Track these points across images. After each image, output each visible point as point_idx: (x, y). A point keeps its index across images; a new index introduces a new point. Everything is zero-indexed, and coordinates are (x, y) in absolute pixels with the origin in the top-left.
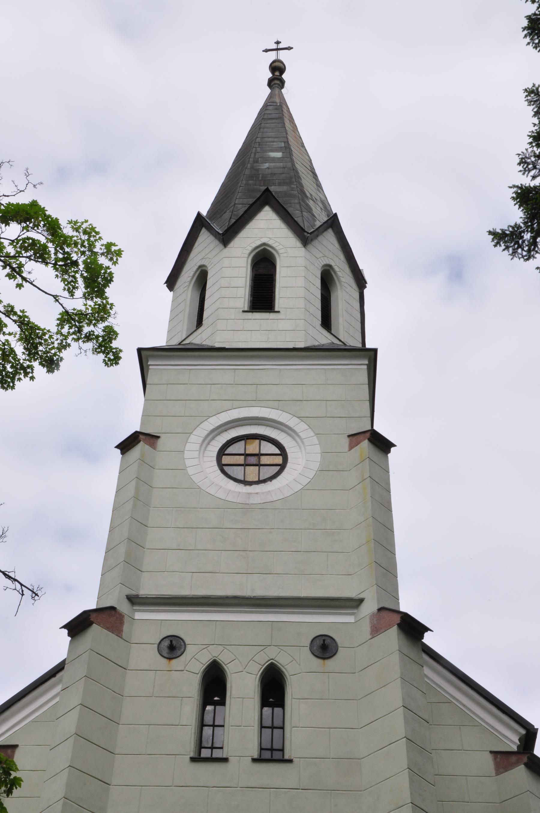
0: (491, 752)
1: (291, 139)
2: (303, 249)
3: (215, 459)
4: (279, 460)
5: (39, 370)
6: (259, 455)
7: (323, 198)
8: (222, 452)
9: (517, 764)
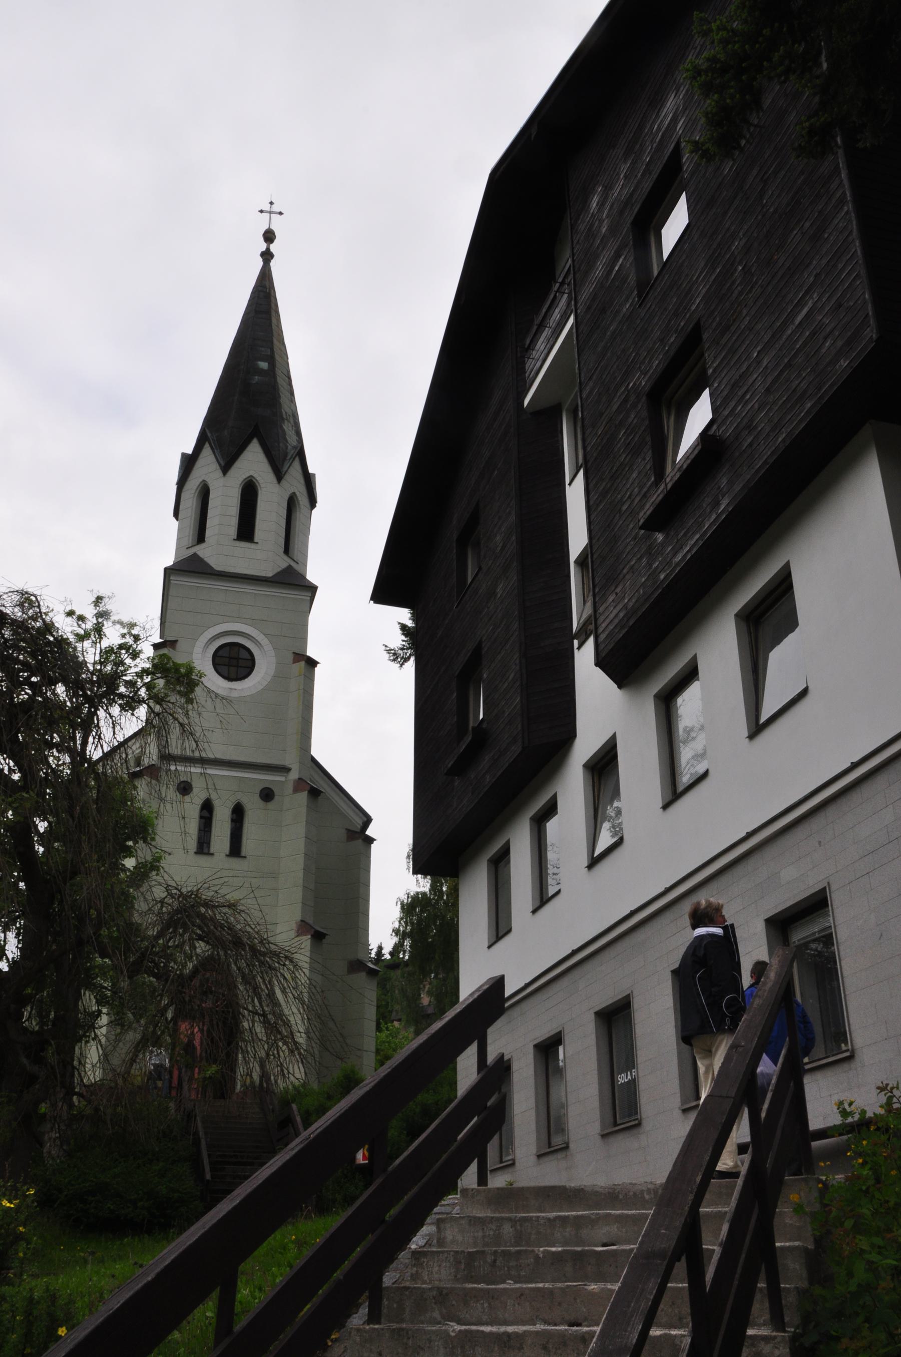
0: (346, 829)
2: (277, 485)
3: (211, 659)
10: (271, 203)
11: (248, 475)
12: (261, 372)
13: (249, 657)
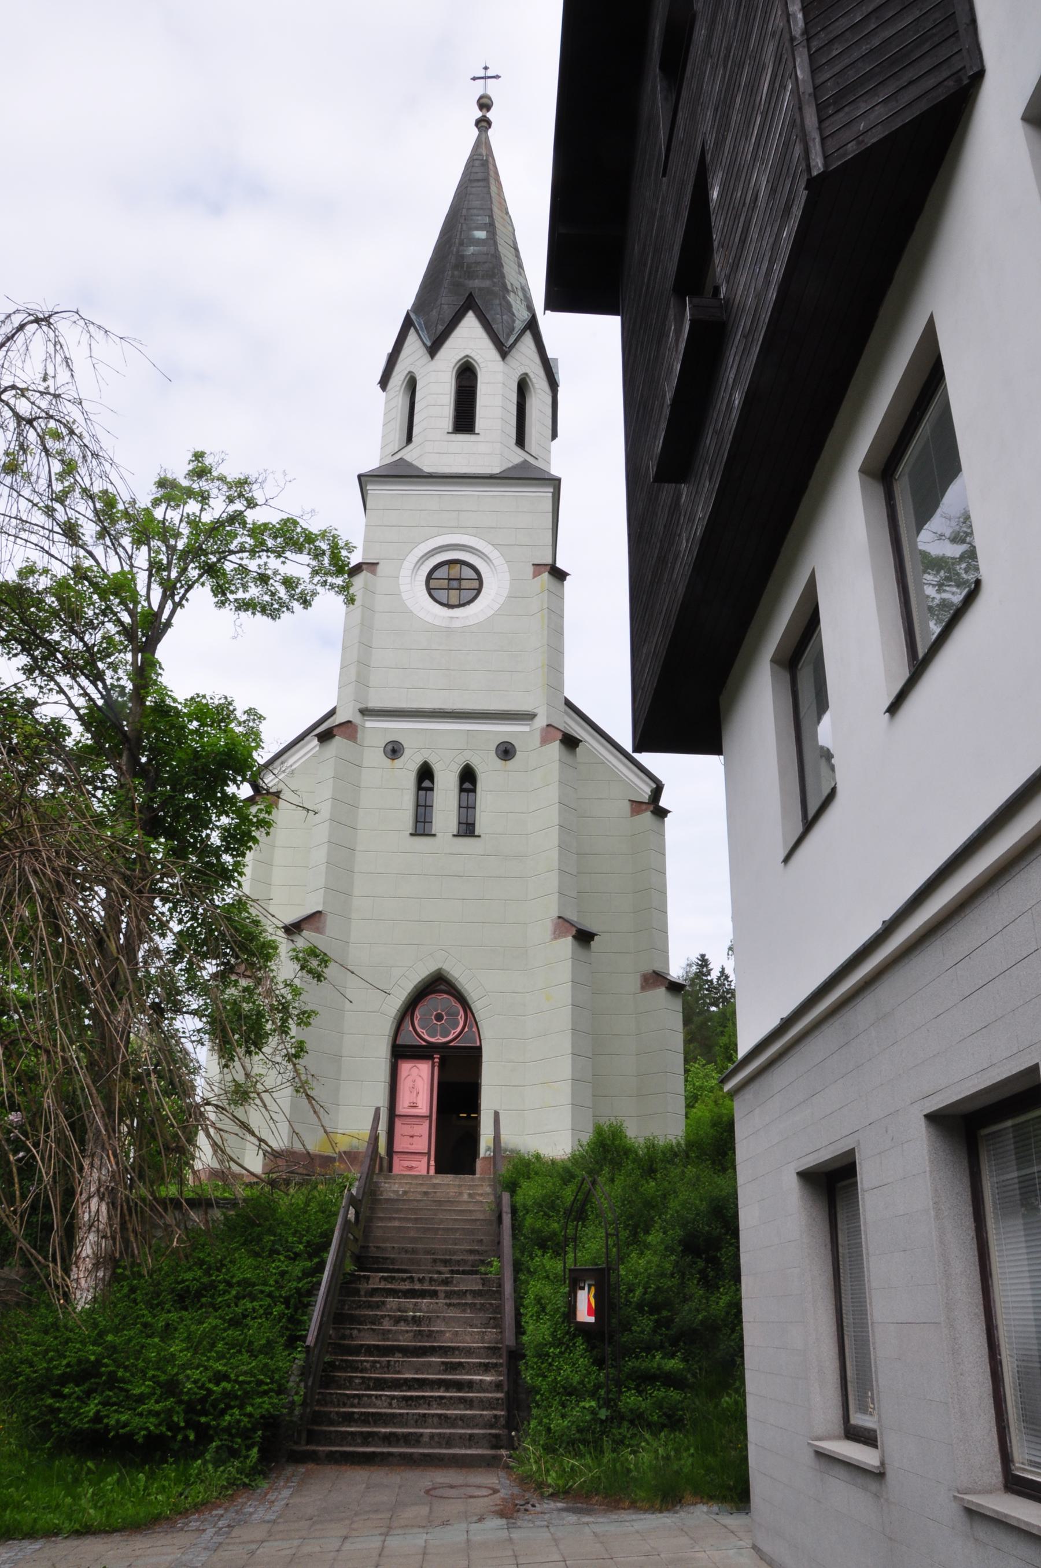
1: (495, 209)
4: (476, 584)
5: (296, 605)
6: (460, 579)
7: (523, 282)
8: (429, 577)
9: (646, 810)
10: (486, 68)
11: (463, 355)
12: (479, 242)
13: (475, 576)
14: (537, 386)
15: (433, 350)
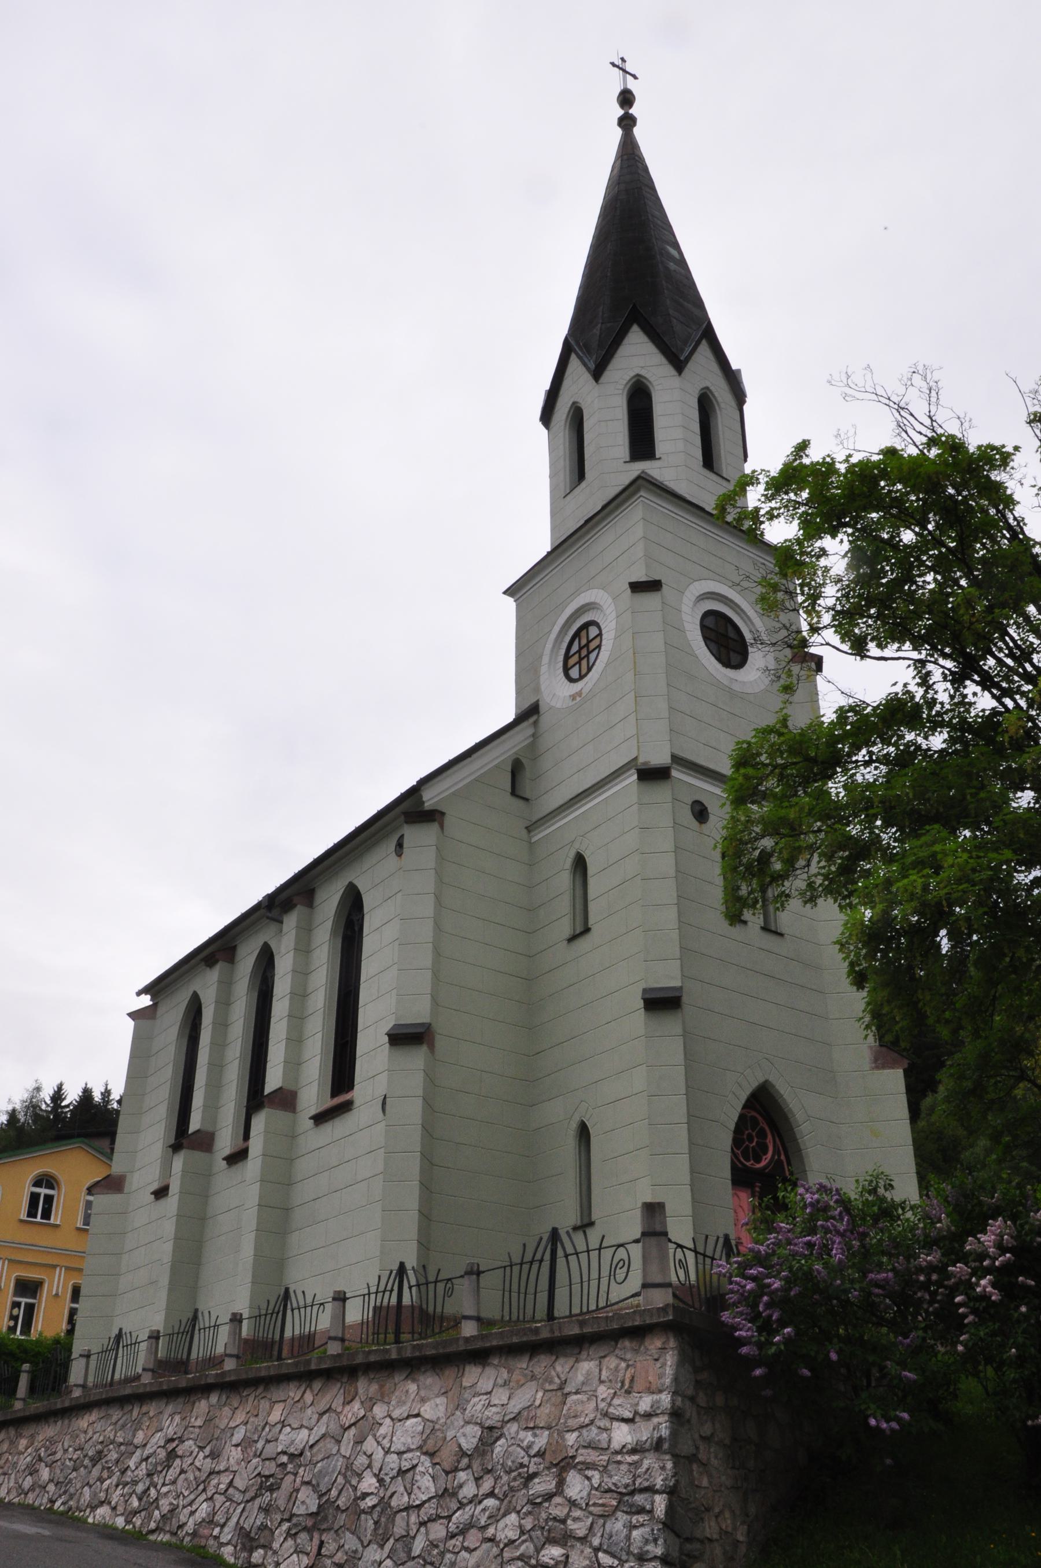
14: (720, 399)
15: (597, 374)
